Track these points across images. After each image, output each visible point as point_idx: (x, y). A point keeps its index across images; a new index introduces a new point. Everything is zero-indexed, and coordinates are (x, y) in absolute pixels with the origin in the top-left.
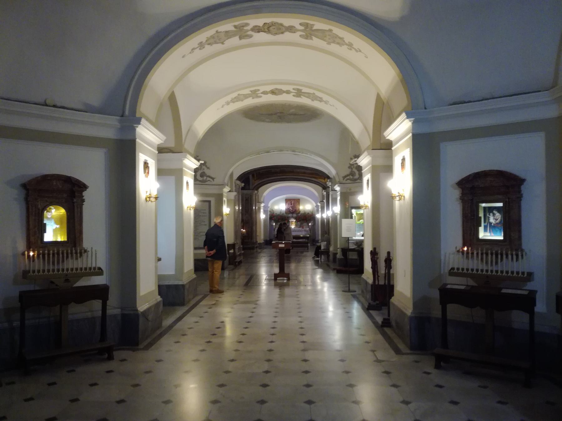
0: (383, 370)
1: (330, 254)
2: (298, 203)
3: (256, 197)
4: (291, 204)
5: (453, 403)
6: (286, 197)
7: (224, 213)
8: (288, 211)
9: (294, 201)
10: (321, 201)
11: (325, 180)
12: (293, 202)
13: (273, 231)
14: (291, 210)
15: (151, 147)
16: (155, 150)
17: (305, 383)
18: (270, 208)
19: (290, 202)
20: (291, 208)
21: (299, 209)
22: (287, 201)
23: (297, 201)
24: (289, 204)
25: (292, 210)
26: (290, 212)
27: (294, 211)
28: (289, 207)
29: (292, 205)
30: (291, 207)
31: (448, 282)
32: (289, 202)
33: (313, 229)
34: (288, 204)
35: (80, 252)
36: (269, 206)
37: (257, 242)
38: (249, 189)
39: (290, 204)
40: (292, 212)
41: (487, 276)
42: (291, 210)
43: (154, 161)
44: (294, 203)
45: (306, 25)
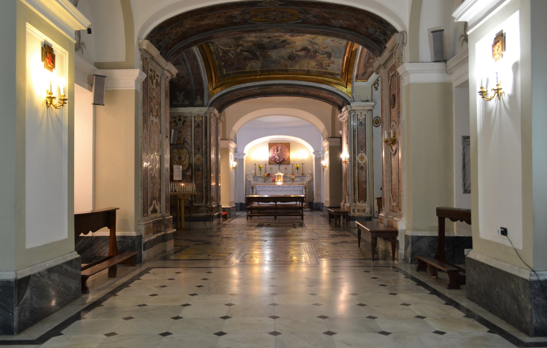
0: (358, 303)
1: (398, 238)
2: (287, 149)
3: (217, 124)
4: (277, 151)
5: (335, 244)
6: (270, 141)
7: (231, 167)
8: (273, 161)
9: (281, 146)
10: (330, 136)
11: (346, 88)
12: (280, 147)
13: (251, 190)
14: (277, 159)
15: (71, 37)
16: (72, 38)
17: (272, 330)
18: (246, 155)
19: (276, 148)
20: (276, 157)
21: (289, 158)
22: (271, 145)
23: (287, 146)
24: (274, 151)
25: (278, 160)
26: (276, 162)
27: (282, 161)
28: (274, 155)
29: (279, 152)
30: (277, 154)
31: (309, 213)
32: (275, 147)
33: (309, 188)
34: (273, 151)
35: (205, 187)
36: (244, 153)
37: (219, 206)
38: (202, 105)
39: (276, 150)
40: (278, 162)
41: (184, 194)
42: (277, 159)
43: (67, 53)
44: (281, 149)
45: (322, 68)
